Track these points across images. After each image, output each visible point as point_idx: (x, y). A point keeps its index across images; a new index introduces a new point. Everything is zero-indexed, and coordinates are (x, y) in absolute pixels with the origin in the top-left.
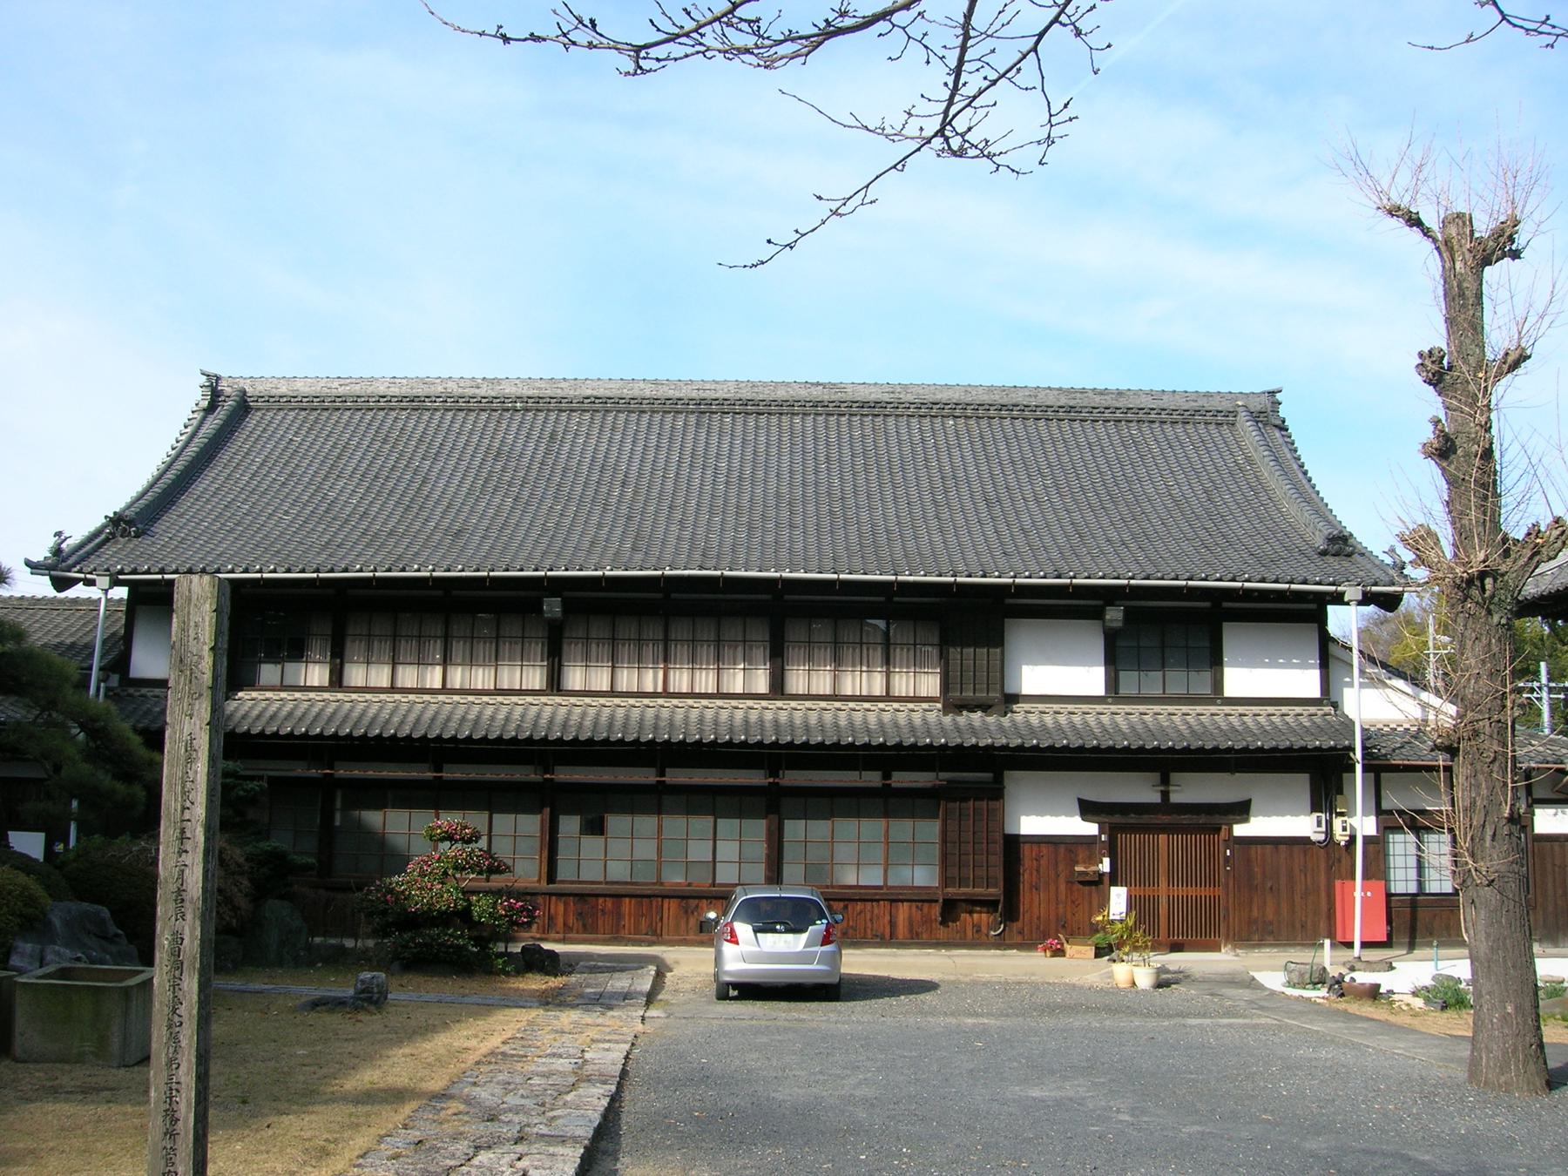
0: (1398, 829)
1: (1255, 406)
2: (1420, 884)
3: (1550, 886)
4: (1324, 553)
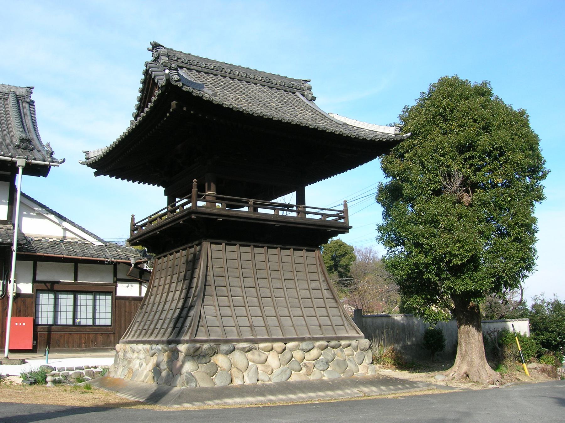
0: (43, 291)
1: (19, 92)
2: (55, 318)
3: (123, 322)
4: (18, 147)
